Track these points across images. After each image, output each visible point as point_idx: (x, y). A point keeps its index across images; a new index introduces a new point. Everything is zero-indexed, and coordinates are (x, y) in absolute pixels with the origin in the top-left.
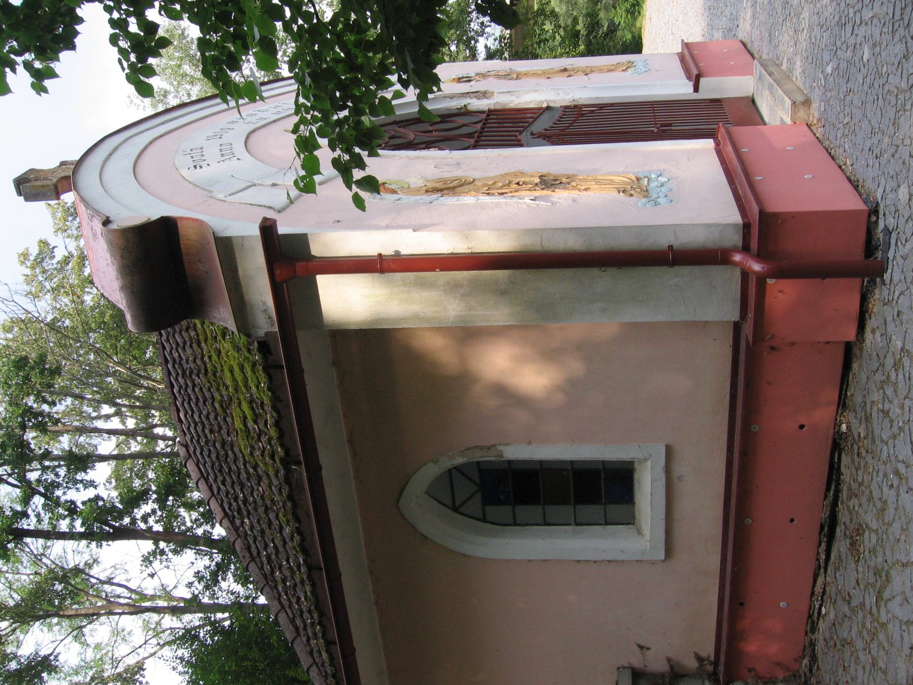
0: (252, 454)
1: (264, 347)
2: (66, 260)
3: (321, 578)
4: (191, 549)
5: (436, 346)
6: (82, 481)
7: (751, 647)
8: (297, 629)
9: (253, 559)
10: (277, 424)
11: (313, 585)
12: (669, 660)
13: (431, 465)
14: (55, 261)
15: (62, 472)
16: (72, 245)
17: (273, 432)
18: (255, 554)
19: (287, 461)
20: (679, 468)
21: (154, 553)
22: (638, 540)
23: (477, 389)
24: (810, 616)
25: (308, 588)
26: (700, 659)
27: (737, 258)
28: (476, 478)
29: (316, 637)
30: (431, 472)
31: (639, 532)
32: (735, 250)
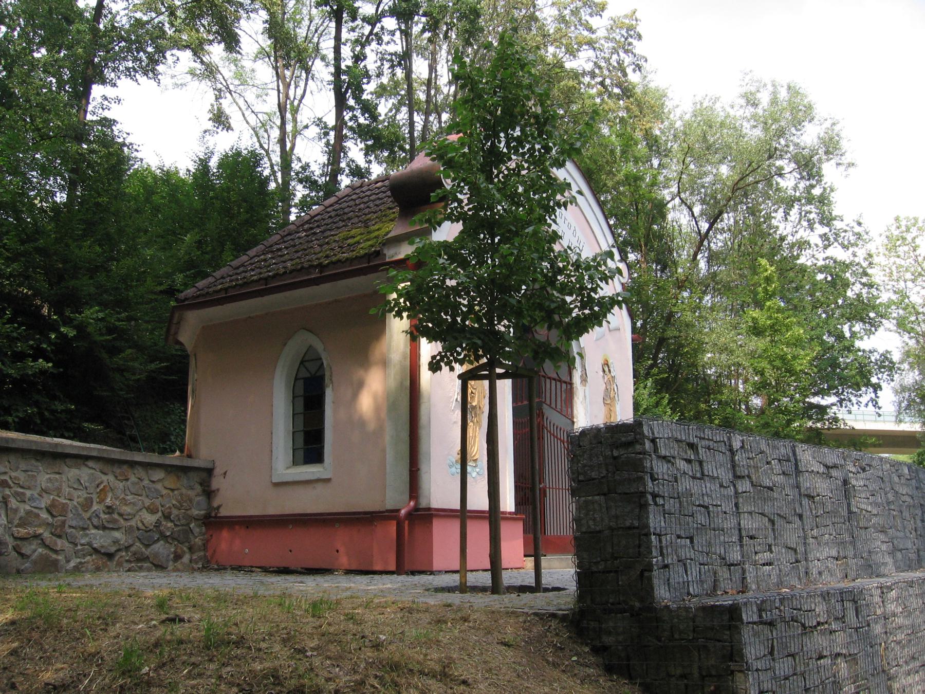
0: (335, 241)
1: (378, 254)
2: (591, 30)
3: (262, 285)
4: (329, 160)
5: (379, 350)
6: (382, 64)
7: (225, 534)
8: (238, 268)
9: (283, 237)
10: (339, 261)
11: (256, 281)
12: (218, 490)
13: (322, 347)
14: (588, 18)
15: (392, 48)
16: (601, 33)
17: (334, 259)
18: (285, 239)
19: (321, 267)
20: (319, 486)
21: (326, 127)
22: (283, 467)
23: (361, 372)
24: (240, 567)
25: (255, 278)
26: (219, 507)
27: (412, 503)
28: (318, 374)
29: (231, 281)
30: (319, 346)
31: (288, 468)
32: (417, 503)
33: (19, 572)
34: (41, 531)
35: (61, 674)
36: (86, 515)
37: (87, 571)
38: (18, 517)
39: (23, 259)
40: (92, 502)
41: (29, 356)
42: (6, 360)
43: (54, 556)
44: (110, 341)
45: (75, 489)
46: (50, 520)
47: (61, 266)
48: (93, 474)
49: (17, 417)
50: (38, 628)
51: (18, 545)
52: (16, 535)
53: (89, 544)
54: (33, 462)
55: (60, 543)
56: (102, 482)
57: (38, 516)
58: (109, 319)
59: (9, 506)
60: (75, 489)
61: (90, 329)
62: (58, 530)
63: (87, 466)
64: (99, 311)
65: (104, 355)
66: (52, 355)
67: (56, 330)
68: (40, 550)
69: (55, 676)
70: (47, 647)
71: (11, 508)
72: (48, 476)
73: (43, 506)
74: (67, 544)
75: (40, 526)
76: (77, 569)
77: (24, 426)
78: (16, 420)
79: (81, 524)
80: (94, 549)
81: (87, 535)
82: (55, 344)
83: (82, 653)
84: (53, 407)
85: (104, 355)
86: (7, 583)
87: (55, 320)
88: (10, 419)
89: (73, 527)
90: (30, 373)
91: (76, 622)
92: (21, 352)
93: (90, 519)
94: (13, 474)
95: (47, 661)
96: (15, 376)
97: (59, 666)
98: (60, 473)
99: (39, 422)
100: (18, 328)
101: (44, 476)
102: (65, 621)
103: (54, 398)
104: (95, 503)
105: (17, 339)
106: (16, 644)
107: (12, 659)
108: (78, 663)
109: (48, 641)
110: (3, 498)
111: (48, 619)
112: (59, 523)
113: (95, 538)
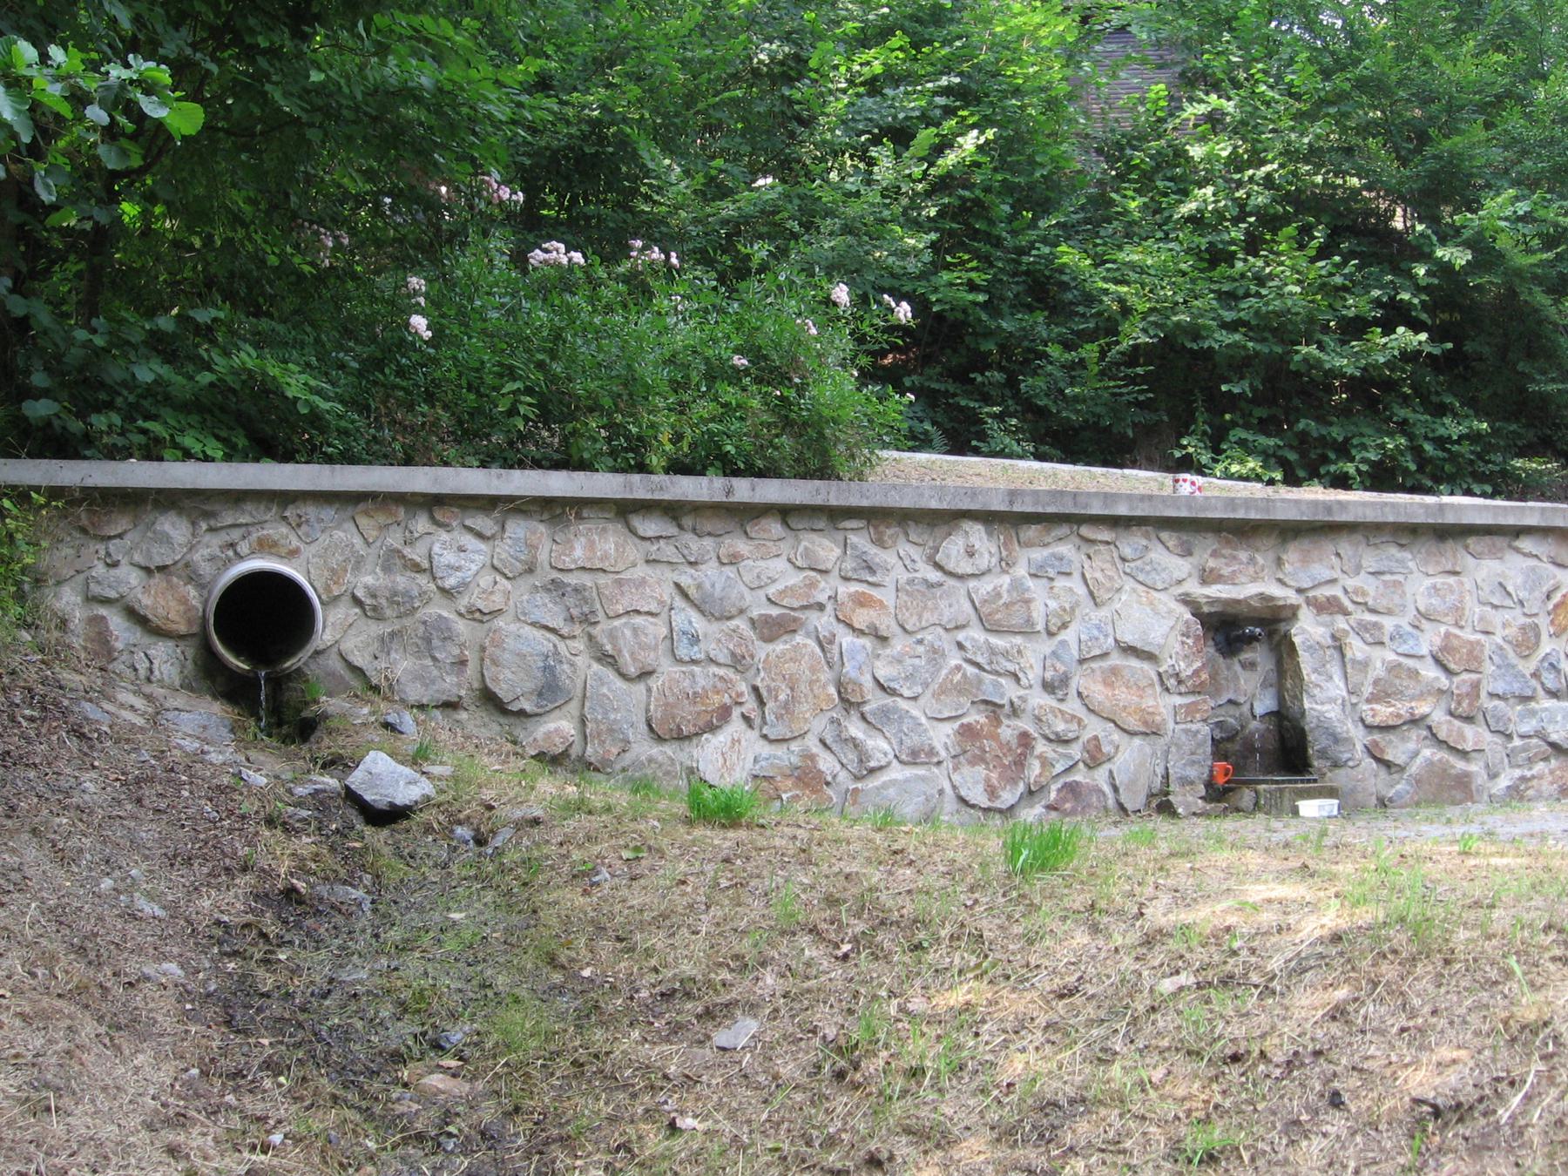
33: (1383, 803)
34: (1422, 708)
35: (1452, 1077)
36: (1528, 667)
37: (1539, 796)
38: (1370, 679)
39: (1332, 110)
40: (1538, 636)
41: (1376, 322)
42: (1326, 339)
43: (1460, 765)
44: (1550, 264)
45: (1495, 607)
46: (1444, 682)
47: (1418, 113)
48: (1533, 569)
49: (1364, 461)
50: (1395, 952)
51: (1376, 743)
52: (1369, 720)
53: (1540, 735)
54: (1393, 551)
55: (1472, 735)
56: (1556, 588)
57: (1414, 674)
58: (1541, 213)
59: (1349, 655)
60: (1495, 607)
61: (1503, 243)
62: (1465, 704)
63: (1517, 550)
64: (1517, 199)
65: (1542, 299)
66: (1424, 316)
67: (1425, 256)
68: (1427, 752)
69: (1438, 1081)
70: (1416, 1002)
71: (1354, 661)
72: (1428, 582)
73: (1425, 651)
74: (1488, 736)
75: (1421, 697)
76: (1516, 793)
77: (1382, 477)
78: (1364, 468)
79: (1516, 687)
80: (1553, 745)
81: (1533, 713)
82: (1426, 289)
83: (1506, 1023)
84: (1441, 431)
85: (1542, 299)
86: (1350, 829)
87: (1422, 234)
88: (1350, 468)
89: (1498, 696)
90: (1382, 360)
91: (1489, 937)
92: (1357, 317)
93: (1535, 675)
94: (1351, 583)
95: (1417, 1036)
96: (1349, 371)
97: (1446, 1053)
98: (1456, 573)
99: (1413, 467)
100: (1345, 263)
101: (1419, 579)
102: (1462, 934)
103: (1440, 410)
104: (1544, 637)
105: (1345, 289)
106: (1342, 993)
107: (1335, 1029)
108: (1494, 1048)
109: (1418, 986)
110: (1333, 637)
111: (1419, 929)
112: (1464, 690)
113: (1552, 721)
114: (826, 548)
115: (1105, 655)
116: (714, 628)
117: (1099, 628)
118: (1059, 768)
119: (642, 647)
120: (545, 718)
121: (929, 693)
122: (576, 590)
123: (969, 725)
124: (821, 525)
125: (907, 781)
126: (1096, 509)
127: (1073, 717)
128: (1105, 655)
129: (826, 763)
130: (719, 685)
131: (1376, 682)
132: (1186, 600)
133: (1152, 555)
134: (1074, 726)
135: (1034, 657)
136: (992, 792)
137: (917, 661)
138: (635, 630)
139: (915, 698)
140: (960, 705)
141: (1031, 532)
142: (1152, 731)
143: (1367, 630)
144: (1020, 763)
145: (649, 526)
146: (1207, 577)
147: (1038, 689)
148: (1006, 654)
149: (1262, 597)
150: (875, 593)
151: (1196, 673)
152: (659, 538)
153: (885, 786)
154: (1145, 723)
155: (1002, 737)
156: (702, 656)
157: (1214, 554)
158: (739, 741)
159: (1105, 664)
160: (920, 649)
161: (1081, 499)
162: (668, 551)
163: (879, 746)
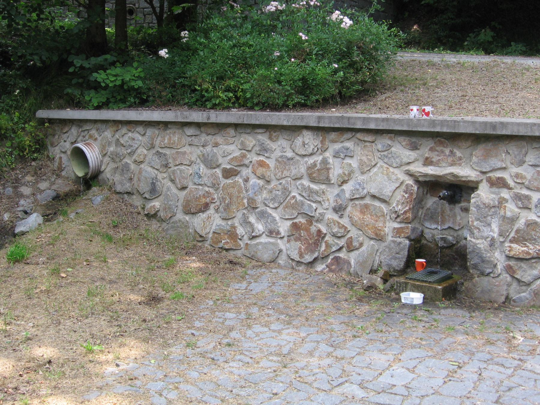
114: (250, 140)
115: (362, 198)
116: (209, 172)
117: (360, 184)
118: (334, 249)
119: (184, 178)
120: (153, 201)
121: (282, 207)
122: (164, 155)
123: (296, 223)
124: (249, 131)
125: (266, 243)
126: (359, 126)
127: (343, 226)
128: (362, 198)
129: (240, 231)
130: (206, 194)
131: (518, 231)
132: (410, 174)
133: (393, 149)
134: (342, 231)
135: (331, 194)
136: (301, 255)
137: (277, 192)
138: (181, 171)
139: (276, 208)
140: (293, 214)
141: (333, 135)
142: (379, 238)
143: (520, 199)
144: (317, 244)
145: (190, 131)
146: (428, 162)
147: (331, 210)
148: (317, 193)
149: (452, 174)
150: (267, 161)
151: (405, 212)
152: (192, 136)
153: (258, 244)
154: (376, 234)
155: (311, 230)
156: (203, 183)
157: (431, 149)
158: (211, 217)
159: (362, 202)
160: (280, 187)
161: (352, 121)
162: (195, 141)
163: (260, 227)
